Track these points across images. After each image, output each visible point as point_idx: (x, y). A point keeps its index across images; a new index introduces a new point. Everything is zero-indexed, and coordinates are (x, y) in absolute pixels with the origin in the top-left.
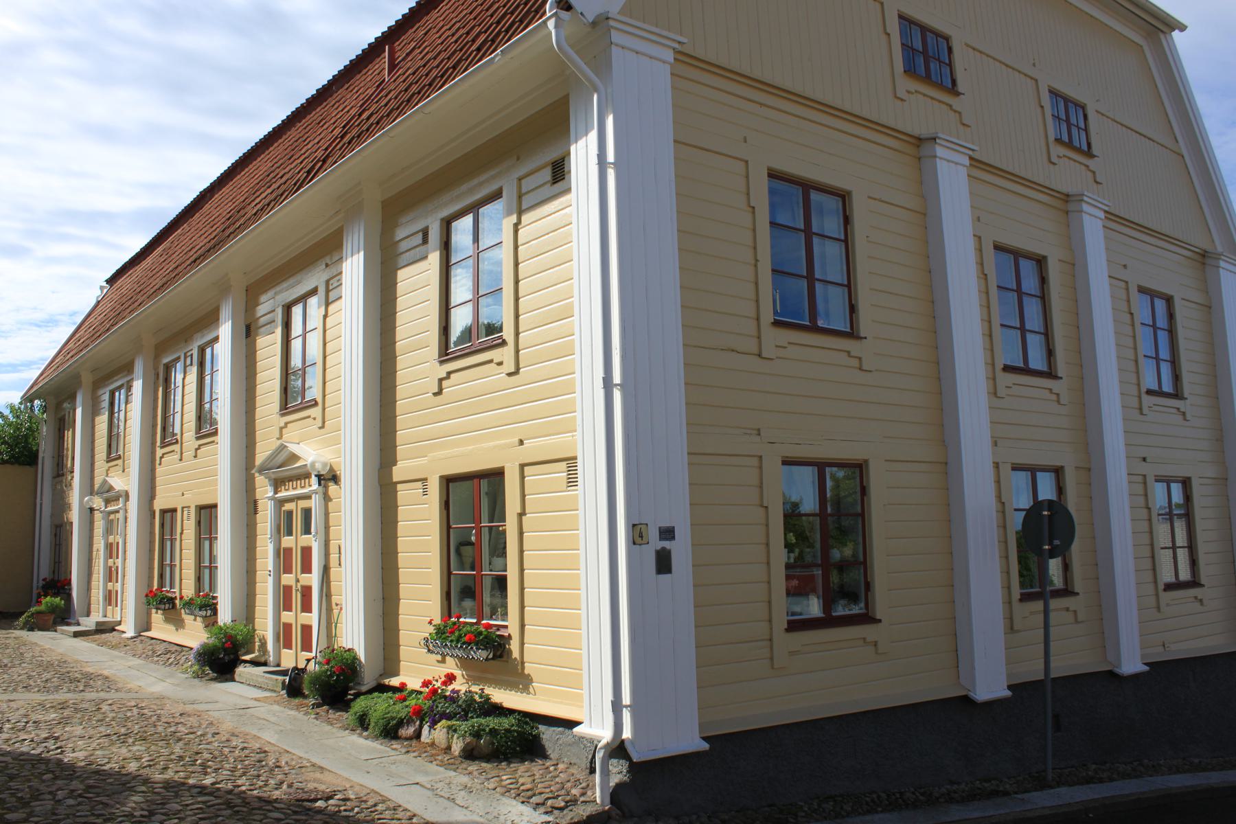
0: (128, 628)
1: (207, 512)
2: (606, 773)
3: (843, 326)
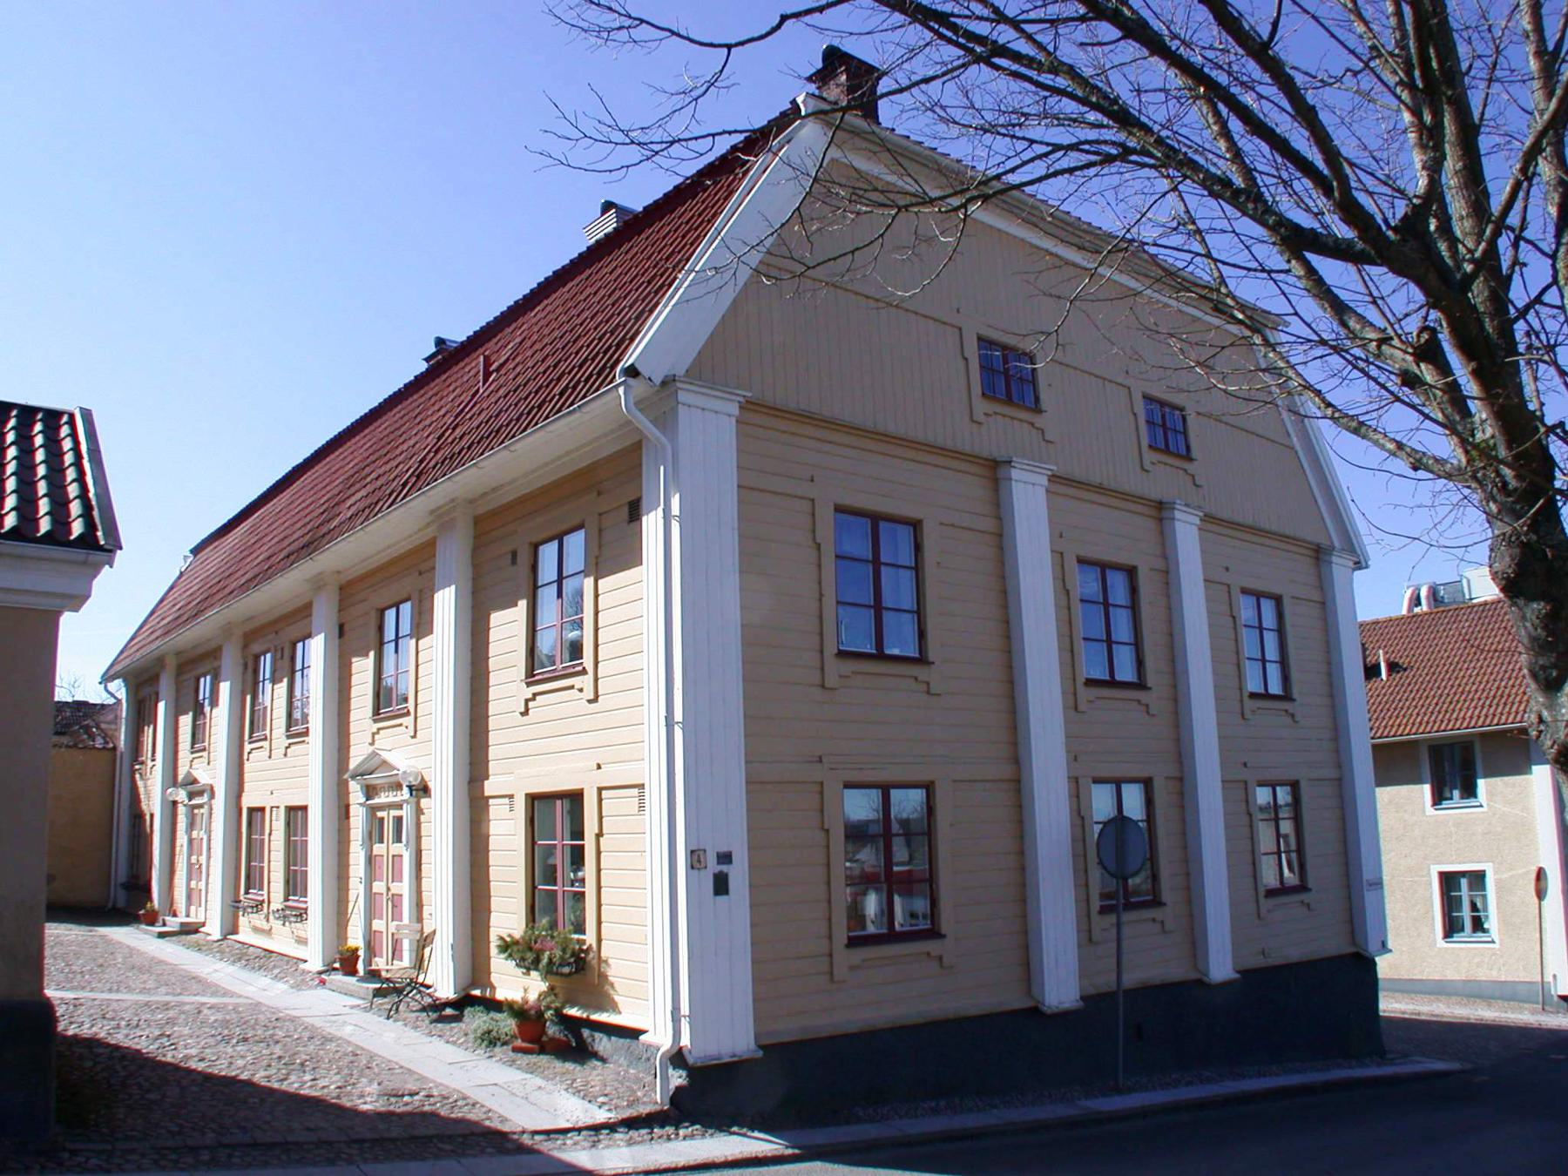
0: (214, 929)
1: (296, 814)
2: (665, 1079)
3: (912, 652)
